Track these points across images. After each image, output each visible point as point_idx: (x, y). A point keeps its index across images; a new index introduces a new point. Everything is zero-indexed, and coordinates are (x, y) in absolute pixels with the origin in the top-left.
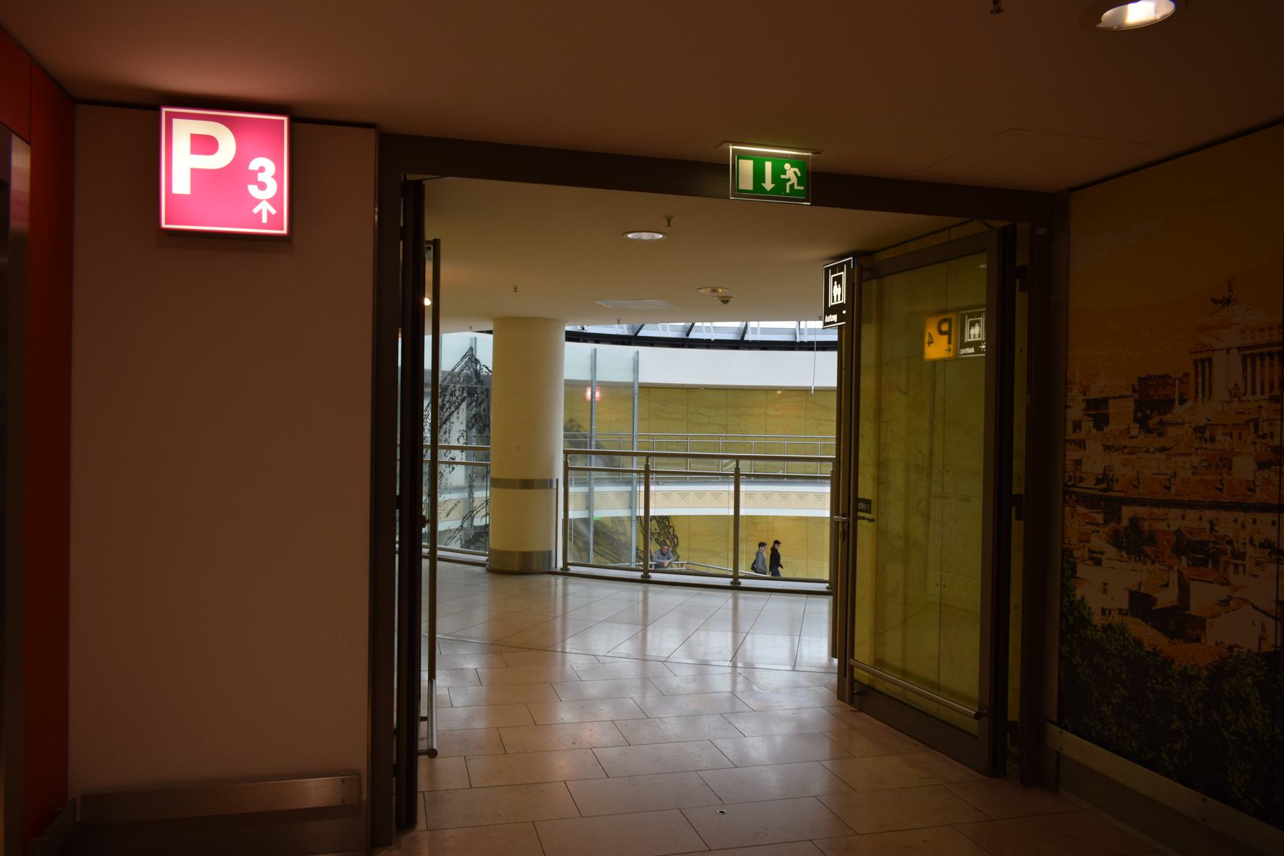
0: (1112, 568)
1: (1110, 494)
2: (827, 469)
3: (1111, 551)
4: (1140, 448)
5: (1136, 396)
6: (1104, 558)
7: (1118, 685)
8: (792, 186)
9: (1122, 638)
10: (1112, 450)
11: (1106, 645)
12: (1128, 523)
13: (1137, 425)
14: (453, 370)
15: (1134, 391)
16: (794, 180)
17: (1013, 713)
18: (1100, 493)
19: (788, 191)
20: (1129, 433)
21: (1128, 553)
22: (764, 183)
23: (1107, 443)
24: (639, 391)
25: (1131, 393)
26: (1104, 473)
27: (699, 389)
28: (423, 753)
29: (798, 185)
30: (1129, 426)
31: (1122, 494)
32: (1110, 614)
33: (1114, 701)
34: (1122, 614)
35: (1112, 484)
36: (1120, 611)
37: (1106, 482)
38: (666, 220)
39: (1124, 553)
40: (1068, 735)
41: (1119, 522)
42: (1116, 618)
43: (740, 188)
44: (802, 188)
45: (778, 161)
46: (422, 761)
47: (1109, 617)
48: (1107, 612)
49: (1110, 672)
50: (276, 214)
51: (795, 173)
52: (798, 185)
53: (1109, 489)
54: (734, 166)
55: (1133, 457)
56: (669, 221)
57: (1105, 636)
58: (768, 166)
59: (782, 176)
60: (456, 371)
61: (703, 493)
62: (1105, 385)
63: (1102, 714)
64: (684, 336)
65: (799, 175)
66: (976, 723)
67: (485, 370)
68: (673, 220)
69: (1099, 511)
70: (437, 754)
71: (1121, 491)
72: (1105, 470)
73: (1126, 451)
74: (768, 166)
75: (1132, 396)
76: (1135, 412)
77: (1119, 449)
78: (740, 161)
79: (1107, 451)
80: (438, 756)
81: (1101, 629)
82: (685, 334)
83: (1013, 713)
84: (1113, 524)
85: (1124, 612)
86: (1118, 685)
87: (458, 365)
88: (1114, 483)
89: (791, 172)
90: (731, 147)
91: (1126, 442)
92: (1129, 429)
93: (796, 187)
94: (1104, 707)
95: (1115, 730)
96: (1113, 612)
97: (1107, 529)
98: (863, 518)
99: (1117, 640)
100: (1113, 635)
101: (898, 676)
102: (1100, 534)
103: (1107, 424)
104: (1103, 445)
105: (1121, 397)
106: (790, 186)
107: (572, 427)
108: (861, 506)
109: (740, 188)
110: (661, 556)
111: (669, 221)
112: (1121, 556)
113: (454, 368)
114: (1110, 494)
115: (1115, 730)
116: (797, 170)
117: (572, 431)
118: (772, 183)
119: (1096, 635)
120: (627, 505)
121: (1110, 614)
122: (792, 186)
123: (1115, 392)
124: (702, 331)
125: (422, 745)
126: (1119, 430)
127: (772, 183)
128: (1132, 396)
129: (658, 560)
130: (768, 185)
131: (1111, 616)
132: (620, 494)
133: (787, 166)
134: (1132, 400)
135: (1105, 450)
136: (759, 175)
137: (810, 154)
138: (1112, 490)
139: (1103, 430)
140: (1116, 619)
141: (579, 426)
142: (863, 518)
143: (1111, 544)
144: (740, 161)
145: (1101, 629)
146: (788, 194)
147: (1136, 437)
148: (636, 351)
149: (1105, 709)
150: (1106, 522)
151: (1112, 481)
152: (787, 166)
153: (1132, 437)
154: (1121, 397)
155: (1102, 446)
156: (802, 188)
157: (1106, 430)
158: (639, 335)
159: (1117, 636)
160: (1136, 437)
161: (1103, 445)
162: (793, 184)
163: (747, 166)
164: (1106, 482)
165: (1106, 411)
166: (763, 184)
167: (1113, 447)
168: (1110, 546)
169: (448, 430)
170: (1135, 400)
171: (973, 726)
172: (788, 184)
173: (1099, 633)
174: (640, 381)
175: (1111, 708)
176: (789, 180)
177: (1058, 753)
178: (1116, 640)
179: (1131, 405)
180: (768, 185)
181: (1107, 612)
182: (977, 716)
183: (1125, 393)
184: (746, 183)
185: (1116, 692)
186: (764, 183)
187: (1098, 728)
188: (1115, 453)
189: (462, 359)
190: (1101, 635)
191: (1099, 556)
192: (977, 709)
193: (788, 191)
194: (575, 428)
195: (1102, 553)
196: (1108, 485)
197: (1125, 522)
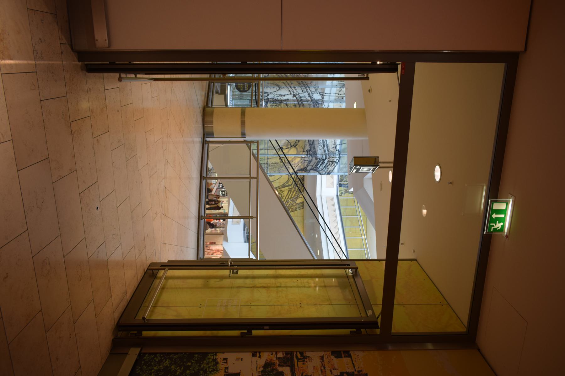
0: (252, 363)
1: (296, 360)
2: (392, 165)
3: (262, 362)
5: (356, 373)
6: (257, 358)
7: (182, 368)
8: (493, 226)
9: (211, 370)
10: (322, 361)
11: (205, 361)
12: (279, 371)
13: (339, 374)
15: (358, 371)
16: (496, 227)
17: (145, 333)
18: (295, 355)
19: (491, 224)
20: (333, 369)
21: (262, 371)
22: (496, 214)
23: (325, 358)
25: (357, 370)
26: (307, 357)
28: (120, 75)
29: (493, 229)
30: (337, 369)
31: (296, 367)
32: (224, 362)
33: (173, 367)
34: (225, 369)
35: (301, 361)
36: (227, 368)
37: (302, 358)
38: (451, 182)
39: (261, 369)
40: (135, 357)
41: (279, 365)
42: (222, 366)
43: (494, 204)
44: (492, 230)
45: (502, 220)
46: (117, 75)
47: (223, 362)
48: (226, 361)
49: (189, 364)
50: (247, 331)
51: (499, 227)
52: (493, 229)
53: (298, 360)
54: (497, 201)
55: (320, 372)
56: (450, 183)
57: (211, 360)
58: (503, 216)
59: (497, 222)
62: (358, 355)
63: (164, 361)
65: (498, 229)
66: (141, 318)
68: (451, 185)
69: (285, 354)
70: (120, 81)
71: (298, 366)
72: (309, 357)
73: (323, 368)
74: (503, 216)
75: (355, 371)
76: (347, 373)
77: (322, 364)
78: (506, 204)
79: (320, 358)
80: (119, 82)
81: (214, 358)
83: (145, 333)
84: (278, 362)
85: (227, 370)
86: (182, 368)
88: (302, 362)
89: (499, 225)
90: (511, 200)
91: (327, 369)
92: (336, 369)
93: (492, 228)
94: (169, 361)
95: (155, 368)
96: (225, 364)
97: (274, 359)
98: (230, 272)
99: (209, 367)
100: (212, 365)
101: (163, 283)
102: (271, 356)
103: (336, 357)
104: (323, 356)
105: (353, 364)
106: (493, 225)
108: (235, 271)
109: (494, 204)
111: (450, 183)
112: (260, 367)
114: (296, 360)
115: (155, 368)
116: (500, 228)
118: (495, 217)
119: (211, 355)
121: (224, 362)
122: (493, 226)
123: (355, 361)
125: (123, 75)
126: (334, 364)
127: (495, 217)
128: (355, 371)
130: (494, 216)
131: (223, 363)
133: (502, 224)
134: (353, 370)
135: (320, 357)
136: (499, 212)
137: (506, 234)
138: (298, 361)
139: (332, 355)
140: (222, 366)
142: (230, 272)
143: (266, 361)
144: (506, 204)
145: (214, 358)
146: (490, 224)
147: (332, 374)
149: (167, 362)
150: (279, 359)
151: (303, 361)
152: (502, 224)
153: (331, 371)
154: (353, 364)
155: (323, 355)
156: (492, 230)
157: (333, 357)
159: (211, 367)
160: (332, 374)
161: (323, 356)
162: (494, 226)
163: (503, 207)
164: (302, 358)
165: (343, 357)
166: (495, 214)
167: (323, 361)
168: (265, 362)
170: (354, 372)
171: (140, 317)
172: (494, 224)
173: (212, 357)
175: (168, 365)
176: (496, 225)
177: (127, 354)
178: (209, 367)
179: (350, 370)
180: (494, 216)
181: (226, 361)
182: (144, 318)
183: (356, 367)
184: (496, 206)
185: (178, 368)
186: (496, 214)
187: (155, 358)
188: (320, 362)
190: (211, 358)
191: (258, 355)
192: (147, 318)
193: (491, 224)
195: (260, 357)
196: (300, 359)
197: (280, 369)
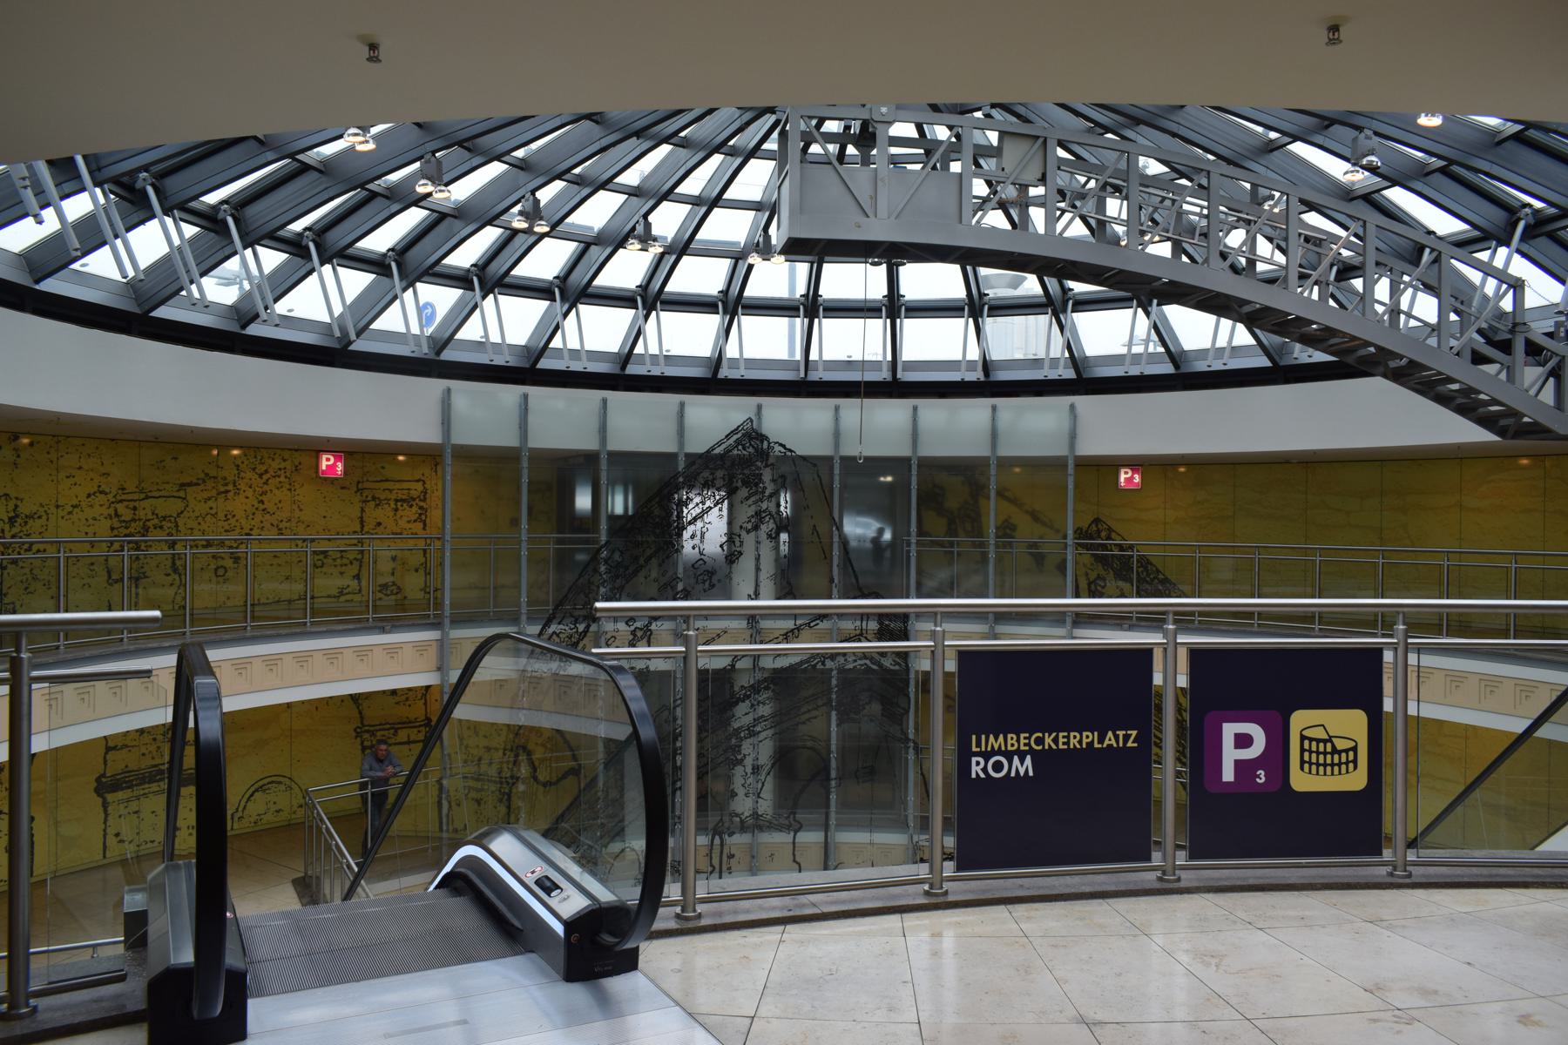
0: (1469, 964)
4: (137, 587)
14: (708, 452)
24: (1076, 471)
27: (1288, 462)
60: (717, 451)
61: (309, 654)
64: (617, 371)
67: (777, 448)
82: (619, 367)
87: (719, 444)
107: (1099, 532)
110: (375, 765)
113: (713, 448)
117: (1099, 537)
120: (433, 663)
124: (579, 359)
129: (372, 773)
132: (420, 647)
141: (1110, 530)
148: (1070, 403)
158: (539, 366)
169: (698, 533)
174: (1077, 454)
189: (728, 437)
194: (1103, 534)
